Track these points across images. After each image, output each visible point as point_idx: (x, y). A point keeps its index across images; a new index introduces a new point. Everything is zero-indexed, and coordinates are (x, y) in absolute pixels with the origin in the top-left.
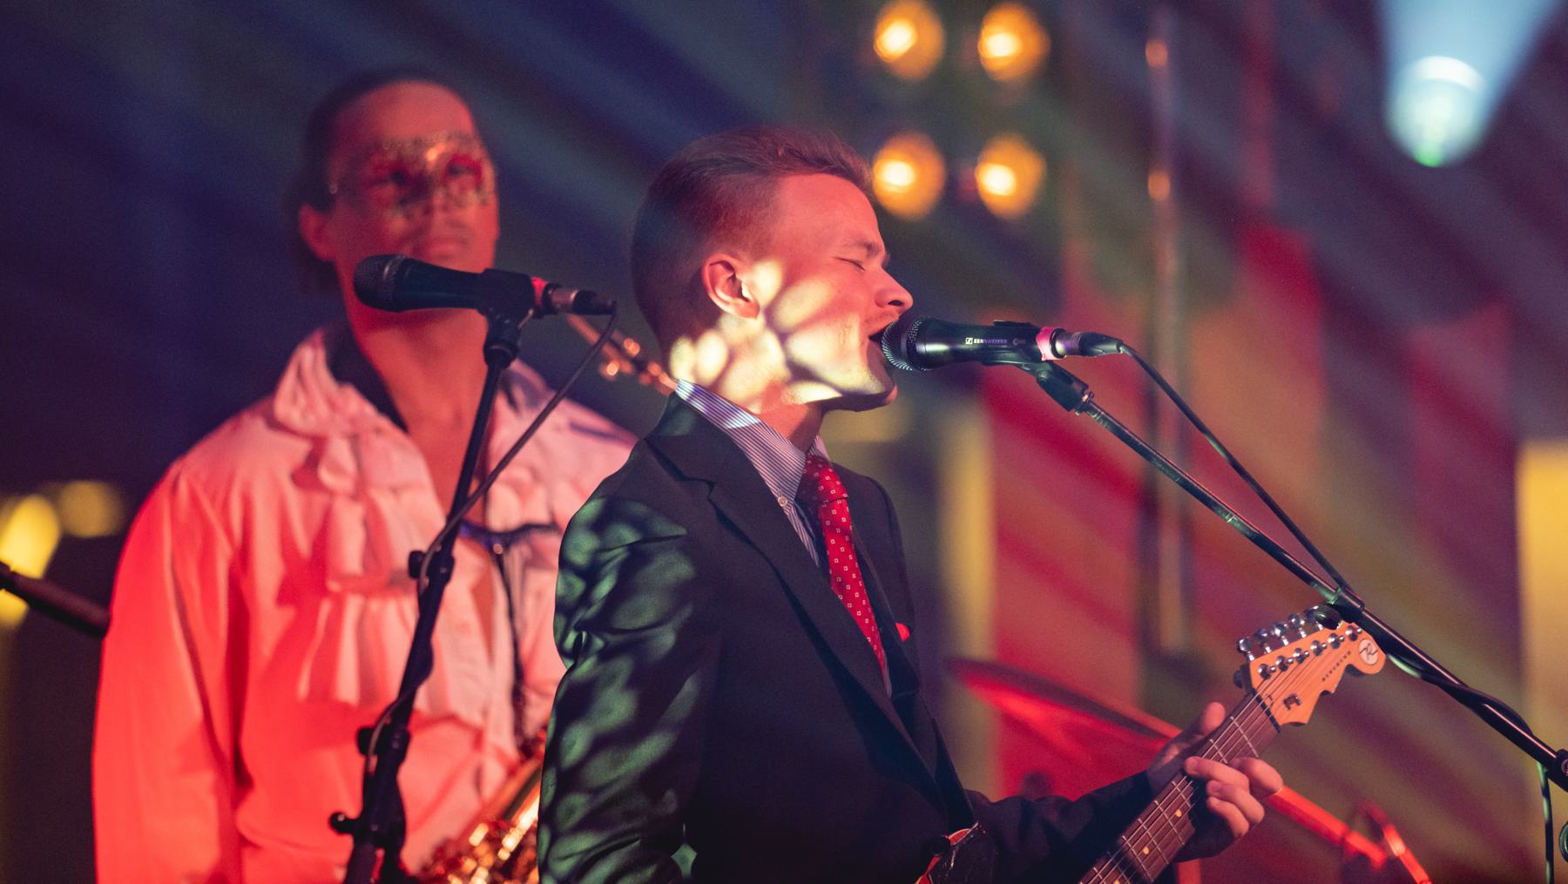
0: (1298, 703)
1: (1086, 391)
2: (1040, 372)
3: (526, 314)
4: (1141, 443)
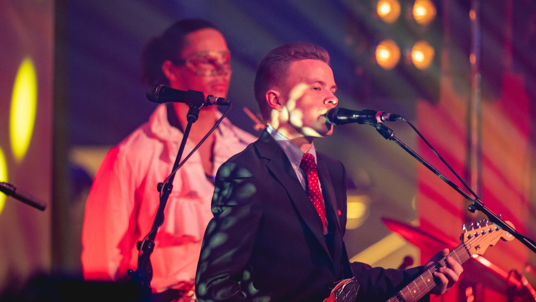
0: (479, 248)
1: (392, 133)
2: (377, 126)
3: (202, 105)
4: (410, 150)
